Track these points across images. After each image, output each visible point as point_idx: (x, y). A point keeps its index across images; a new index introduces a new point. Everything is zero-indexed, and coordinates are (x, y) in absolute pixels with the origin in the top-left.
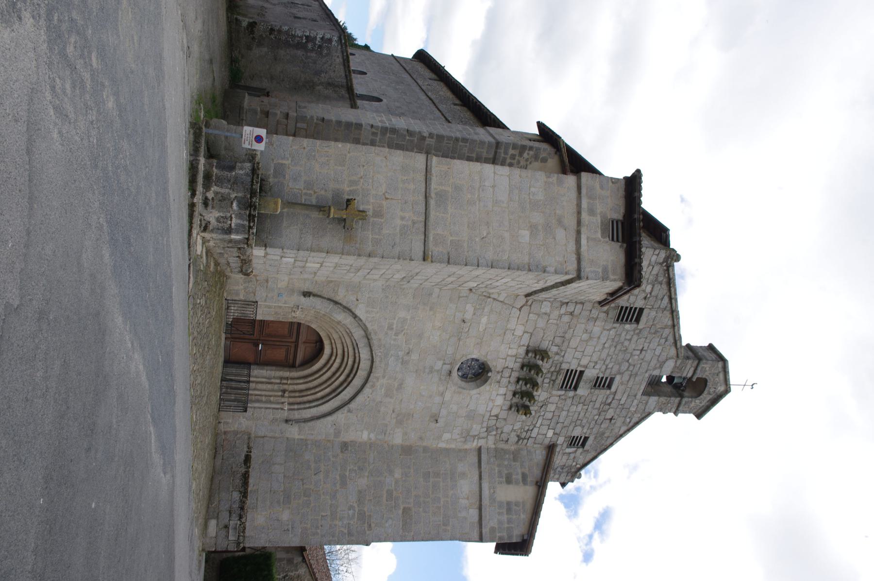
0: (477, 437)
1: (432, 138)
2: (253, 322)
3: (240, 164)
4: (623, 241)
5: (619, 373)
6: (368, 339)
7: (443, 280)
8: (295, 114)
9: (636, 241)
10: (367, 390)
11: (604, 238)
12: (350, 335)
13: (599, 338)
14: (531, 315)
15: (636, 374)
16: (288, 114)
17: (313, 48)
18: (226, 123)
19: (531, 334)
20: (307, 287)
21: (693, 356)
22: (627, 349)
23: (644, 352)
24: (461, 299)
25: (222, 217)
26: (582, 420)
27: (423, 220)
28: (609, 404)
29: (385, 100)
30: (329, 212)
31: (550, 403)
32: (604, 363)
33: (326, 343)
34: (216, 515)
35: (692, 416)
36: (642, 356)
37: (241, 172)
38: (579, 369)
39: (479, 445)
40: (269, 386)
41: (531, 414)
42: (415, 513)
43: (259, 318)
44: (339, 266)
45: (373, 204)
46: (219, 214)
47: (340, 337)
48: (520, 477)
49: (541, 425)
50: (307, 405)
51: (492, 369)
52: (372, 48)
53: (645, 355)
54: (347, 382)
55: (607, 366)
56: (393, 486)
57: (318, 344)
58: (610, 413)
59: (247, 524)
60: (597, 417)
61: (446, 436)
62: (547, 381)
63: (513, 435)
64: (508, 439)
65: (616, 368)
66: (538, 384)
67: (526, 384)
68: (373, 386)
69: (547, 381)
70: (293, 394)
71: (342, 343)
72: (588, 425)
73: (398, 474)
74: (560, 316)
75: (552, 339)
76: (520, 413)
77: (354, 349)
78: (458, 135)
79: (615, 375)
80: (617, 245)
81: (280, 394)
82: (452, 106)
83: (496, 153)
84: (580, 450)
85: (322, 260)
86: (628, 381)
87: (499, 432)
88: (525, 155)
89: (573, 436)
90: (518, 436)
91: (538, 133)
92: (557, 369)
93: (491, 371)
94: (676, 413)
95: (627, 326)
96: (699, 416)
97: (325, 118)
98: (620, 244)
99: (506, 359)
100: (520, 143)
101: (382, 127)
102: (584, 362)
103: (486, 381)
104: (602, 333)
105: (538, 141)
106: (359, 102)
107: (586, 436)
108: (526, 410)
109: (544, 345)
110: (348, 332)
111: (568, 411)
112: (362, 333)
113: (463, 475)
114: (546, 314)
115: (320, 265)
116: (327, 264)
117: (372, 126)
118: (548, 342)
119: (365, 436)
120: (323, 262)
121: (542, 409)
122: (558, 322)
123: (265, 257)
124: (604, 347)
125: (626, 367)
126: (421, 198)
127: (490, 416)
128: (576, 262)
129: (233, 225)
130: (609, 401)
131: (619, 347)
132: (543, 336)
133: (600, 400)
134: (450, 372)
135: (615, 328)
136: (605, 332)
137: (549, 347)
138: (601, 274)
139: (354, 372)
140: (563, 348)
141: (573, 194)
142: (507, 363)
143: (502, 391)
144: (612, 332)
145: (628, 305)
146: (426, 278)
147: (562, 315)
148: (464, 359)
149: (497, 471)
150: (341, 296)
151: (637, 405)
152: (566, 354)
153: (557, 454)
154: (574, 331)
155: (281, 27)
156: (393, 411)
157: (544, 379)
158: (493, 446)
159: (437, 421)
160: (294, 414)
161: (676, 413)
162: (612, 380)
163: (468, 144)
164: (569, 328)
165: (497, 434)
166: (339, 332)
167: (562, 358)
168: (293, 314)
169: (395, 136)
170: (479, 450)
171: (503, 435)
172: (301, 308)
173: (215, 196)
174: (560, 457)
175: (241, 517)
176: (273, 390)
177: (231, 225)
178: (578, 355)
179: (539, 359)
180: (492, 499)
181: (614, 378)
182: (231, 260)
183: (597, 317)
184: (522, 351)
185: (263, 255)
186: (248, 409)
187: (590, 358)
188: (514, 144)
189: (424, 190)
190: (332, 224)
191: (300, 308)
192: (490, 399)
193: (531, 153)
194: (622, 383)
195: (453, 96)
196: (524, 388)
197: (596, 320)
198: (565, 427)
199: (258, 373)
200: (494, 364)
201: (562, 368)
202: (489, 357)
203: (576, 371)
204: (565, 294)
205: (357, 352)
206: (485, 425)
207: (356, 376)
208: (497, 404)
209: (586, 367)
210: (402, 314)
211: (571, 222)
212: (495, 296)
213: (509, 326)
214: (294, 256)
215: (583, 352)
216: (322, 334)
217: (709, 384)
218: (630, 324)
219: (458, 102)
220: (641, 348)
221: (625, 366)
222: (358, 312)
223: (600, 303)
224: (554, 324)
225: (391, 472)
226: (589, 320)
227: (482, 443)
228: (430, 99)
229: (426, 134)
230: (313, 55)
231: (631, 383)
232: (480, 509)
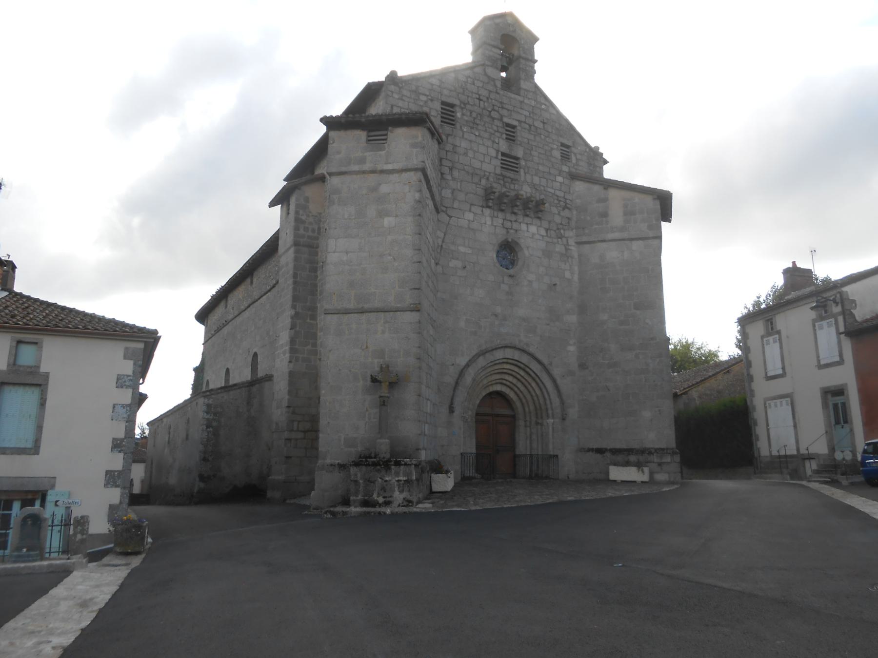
0: (567, 246)
2: (478, 455)
3: (353, 477)
4: (387, 130)
5: (501, 120)
6: (486, 352)
8: (286, 432)
10: (532, 350)
12: (484, 368)
13: (471, 141)
14: (455, 206)
15: (501, 103)
16: (286, 439)
18: (313, 492)
19: (472, 205)
20: (445, 410)
22: (480, 114)
23: (481, 98)
25: (399, 488)
27: (383, 313)
28: (530, 126)
29: (255, 350)
30: (385, 397)
31: (532, 180)
32: (494, 134)
33: (492, 389)
36: (485, 99)
37: (359, 475)
38: (500, 157)
39: (573, 244)
41: (543, 200)
43: (474, 451)
46: (397, 491)
47: (486, 377)
49: (552, 188)
52: (197, 363)
53: (484, 96)
54: (525, 368)
55: (496, 131)
59: (656, 447)
60: (542, 136)
62: (512, 187)
63: (562, 213)
64: (567, 218)
65: (497, 123)
66: (516, 195)
67: (517, 206)
69: (512, 187)
71: (491, 375)
72: (550, 145)
73: (605, 317)
74: (454, 179)
75: (474, 185)
76: (543, 209)
77: (495, 364)
78: (290, 281)
79: (503, 123)
80: (391, 136)
84: (573, 149)
86: (508, 110)
87: (561, 226)
88: (304, 218)
89: (560, 158)
90: (564, 209)
91: (280, 205)
92: (501, 178)
95: (459, 115)
97: (286, 405)
98: (389, 133)
99: (495, 226)
100: (293, 224)
101: (290, 353)
102: (493, 153)
103: (517, 243)
104: (466, 139)
105: (288, 205)
106: (261, 374)
107: (560, 144)
108: (542, 203)
109: (481, 192)
110: (481, 370)
111: (538, 164)
112: (481, 358)
114: (452, 193)
115: (428, 402)
117: (290, 362)
118: (478, 189)
119: (572, 348)
121: (538, 188)
122: (459, 180)
123: (426, 450)
124: (479, 136)
125: (496, 113)
126: (364, 317)
127: (547, 236)
128: (408, 173)
129: (405, 479)
130: (527, 126)
131: (478, 121)
132: (473, 193)
134: (510, 276)
135: (461, 127)
137: (482, 187)
138: (418, 149)
139: (516, 363)
140: (482, 174)
141: (347, 178)
142: (499, 225)
143: (524, 227)
145: (439, 116)
147: (452, 178)
148: (498, 265)
149: (597, 226)
150: (450, 380)
151: (529, 99)
152: (488, 170)
153: (578, 171)
156: (548, 325)
157: (512, 190)
158: (574, 231)
159: (554, 285)
162: (508, 125)
163: (299, 272)
164: (464, 170)
165: (563, 229)
166: (482, 378)
167: (492, 174)
168: (469, 420)
171: (564, 223)
173: (382, 495)
174: (580, 168)
175: (650, 453)
177: (404, 481)
179: (494, 196)
180: (622, 229)
183: (452, 144)
184: (487, 212)
185: (424, 451)
187: (489, 148)
189: (356, 315)
192: (532, 238)
193: (301, 212)
196: (521, 207)
197: (455, 146)
198: (553, 166)
199: (522, 447)
201: (500, 173)
204: (435, 178)
205: (497, 362)
206: (555, 240)
207: (520, 360)
208: (536, 230)
209: (498, 151)
210: (462, 324)
211: (372, 179)
212: (440, 241)
213: (466, 226)
215: (484, 155)
216: (484, 394)
218: (456, 113)
219: (248, 280)
220: (478, 101)
221: (494, 114)
223: (439, 143)
224: (461, 184)
226: (455, 152)
228: (248, 307)
229: (293, 312)
231: (510, 108)
232: (632, 240)
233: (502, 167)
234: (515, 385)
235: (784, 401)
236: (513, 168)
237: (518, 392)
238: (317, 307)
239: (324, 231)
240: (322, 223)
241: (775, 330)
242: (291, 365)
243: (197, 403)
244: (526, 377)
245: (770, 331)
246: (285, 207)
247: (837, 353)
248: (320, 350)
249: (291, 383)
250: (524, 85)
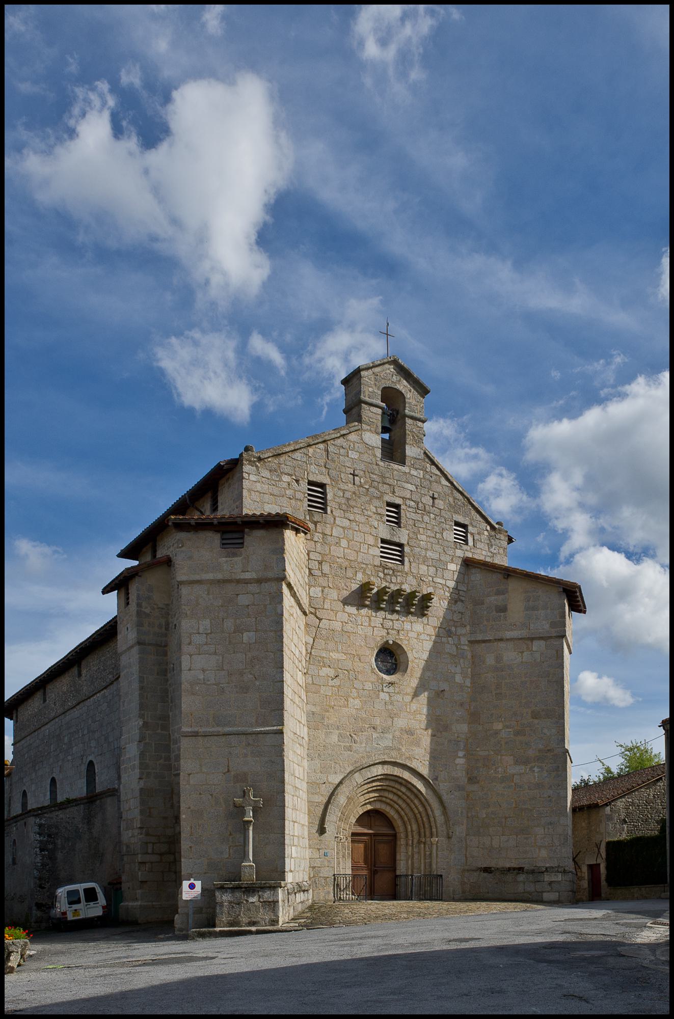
1: (143, 715)
2: (354, 876)
7: (298, 706)
8: (140, 856)
9: (242, 521)
10: (414, 764)
11: (241, 554)
17: (52, 843)
21: (356, 407)
23: (356, 473)
24: (315, 682)
26: (436, 532)
29: (90, 758)
34: (540, 894)
39: (467, 643)
40: (416, 856)
42: (536, 706)
43: (349, 871)
44: (295, 806)
45: (235, 783)
48: (501, 597)
50: (432, 819)
51: (385, 640)
56: (510, 730)
57: (371, 815)
58: (427, 500)
61: (458, 678)
64: (459, 612)
70: (423, 834)
73: (498, 726)
80: (248, 539)
82: (83, 678)
83: (149, 644)
85: (291, 823)
91: (117, 591)
92: (381, 569)
93: (387, 641)
98: (246, 536)
99: (373, 627)
102: (371, 540)
103: (399, 646)
108: (427, 598)
111: (426, 549)
113: (499, 659)
114: (323, 591)
116: (294, 816)
119: (461, 761)
120: (292, 821)
131: (352, 503)
133: (413, 516)
135: (332, 512)
136: (337, 522)
144: (337, 513)
146: (298, 724)
154: (338, 558)
155: (36, 878)
160: (442, 831)
169: (148, 754)
170: (471, 642)
172: (337, 834)
176: (419, 853)
178: (364, 548)
181: (387, 502)
182: (298, 900)
186: (439, 874)
188: (137, 626)
190: (258, 818)
191: (337, 836)
193: (144, 604)
194: (394, 492)
195: (67, 675)
199: (402, 868)
200: (378, 639)
202: (373, 645)
203: (382, 547)
214: (290, 847)
217: (389, 384)
220: (351, 476)
222: (337, 781)
225: (497, 733)
227: (464, 640)
230: (59, 842)
231: (391, 482)
234: (395, 802)
238: (169, 715)
239: (173, 627)
240: (170, 616)
242: (142, 782)
243: (25, 823)
244: (409, 794)
246: (123, 591)
248: (175, 765)
249: (143, 802)
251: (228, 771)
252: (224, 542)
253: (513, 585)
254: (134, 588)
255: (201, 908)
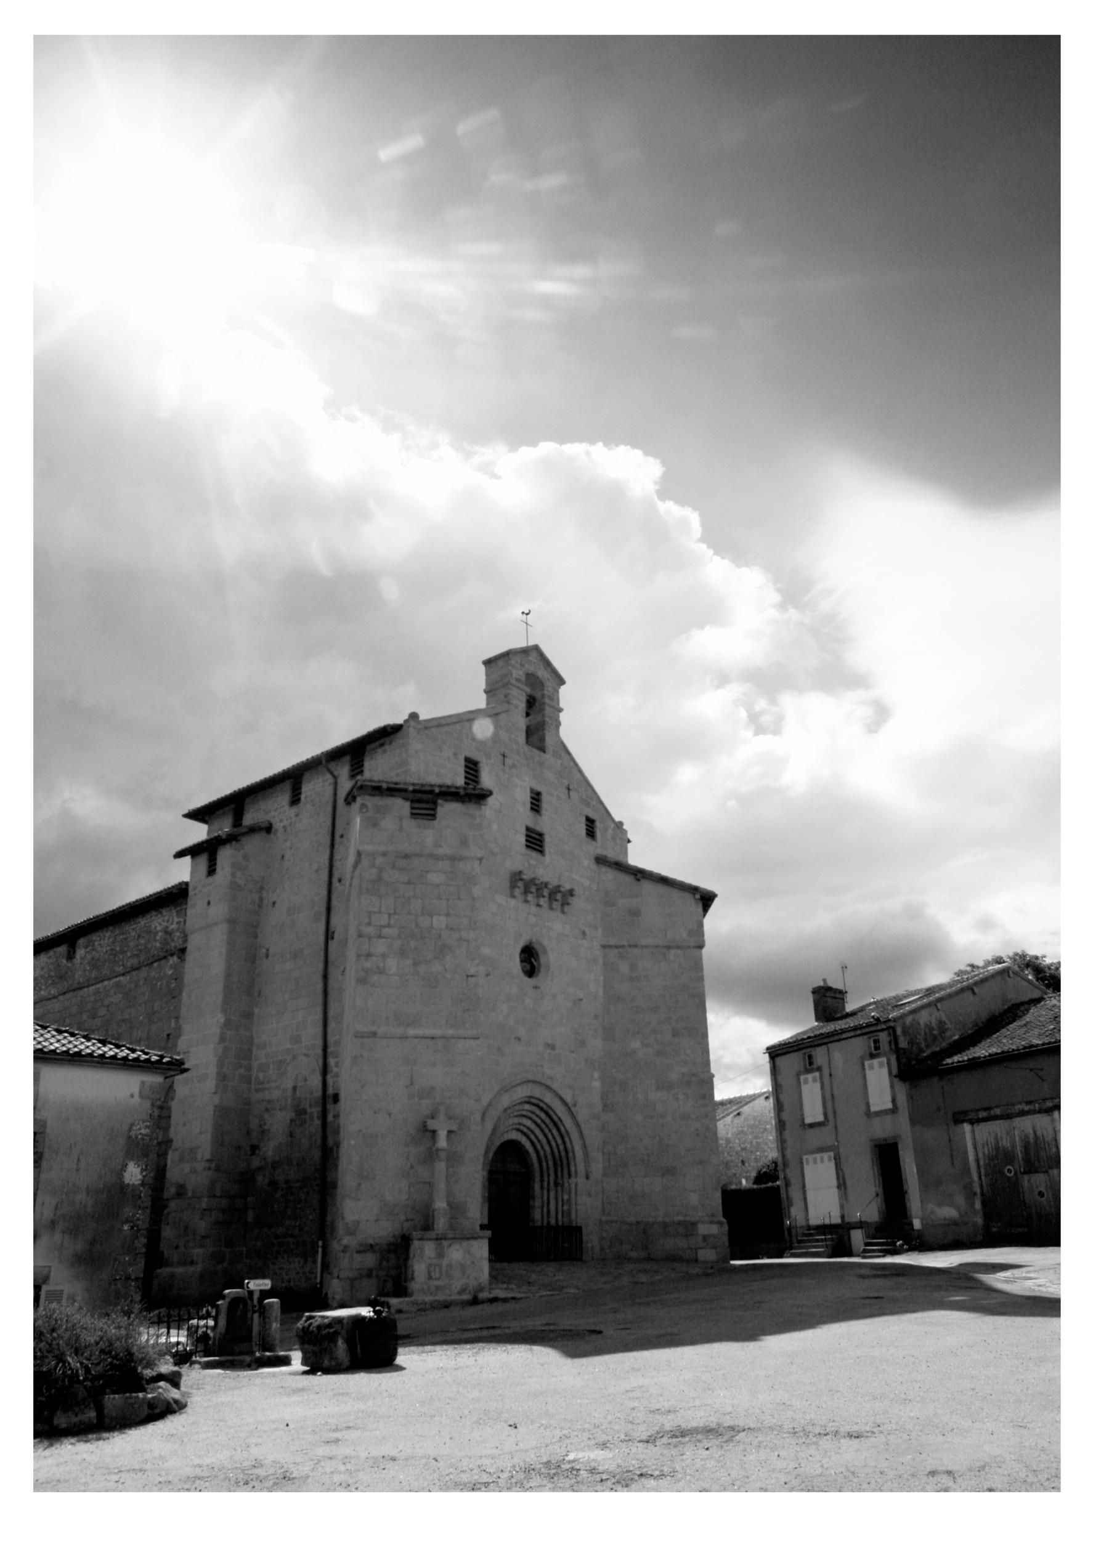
35: (563, 690)
68: (551, 1078)
81: (559, 1189)
94: (560, 710)
96: (562, 682)
119: (596, 1084)
161: (560, 710)
170: (604, 947)
193: (238, 874)
233: (527, 846)
235: (826, 1156)
236: (534, 841)
237: (535, 1141)
241: (815, 1066)
245: (808, 1067)
247: (889, 1098)
250: (549, 740)
251: (412, 1084)
252: (414, 811)
253: (647, 886)
254: (225, 855)
255: (371, 1270)
